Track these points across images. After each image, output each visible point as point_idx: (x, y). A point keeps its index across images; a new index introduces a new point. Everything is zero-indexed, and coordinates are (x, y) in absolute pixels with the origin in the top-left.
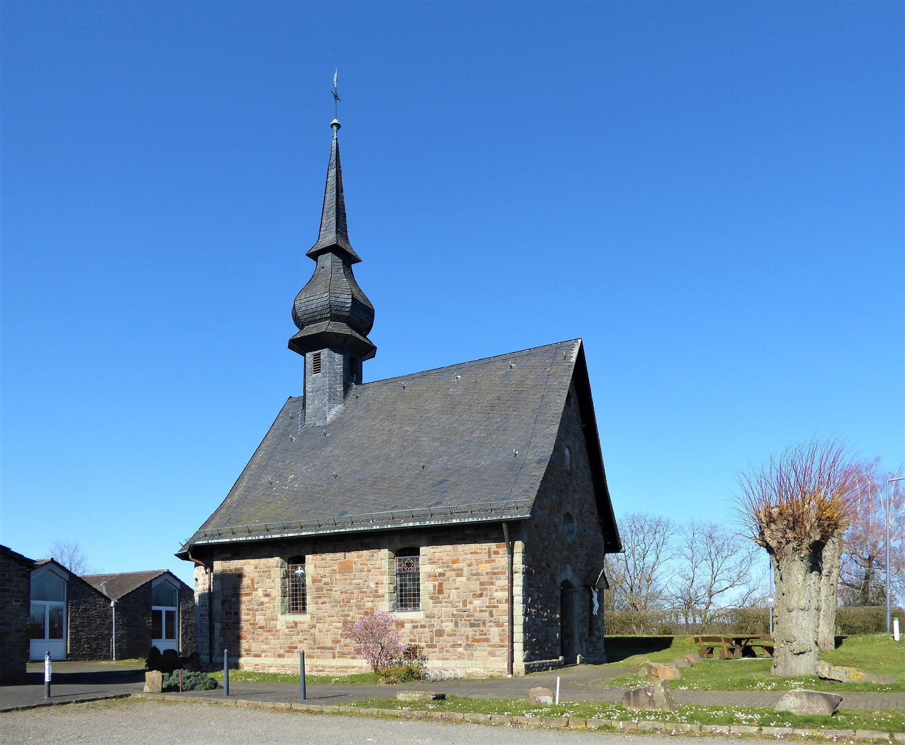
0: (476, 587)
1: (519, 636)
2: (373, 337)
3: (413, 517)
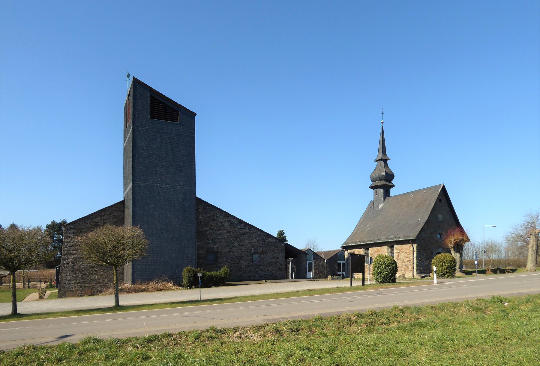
0: (406, 255)
1: (415, 268)
2: (393, 182)
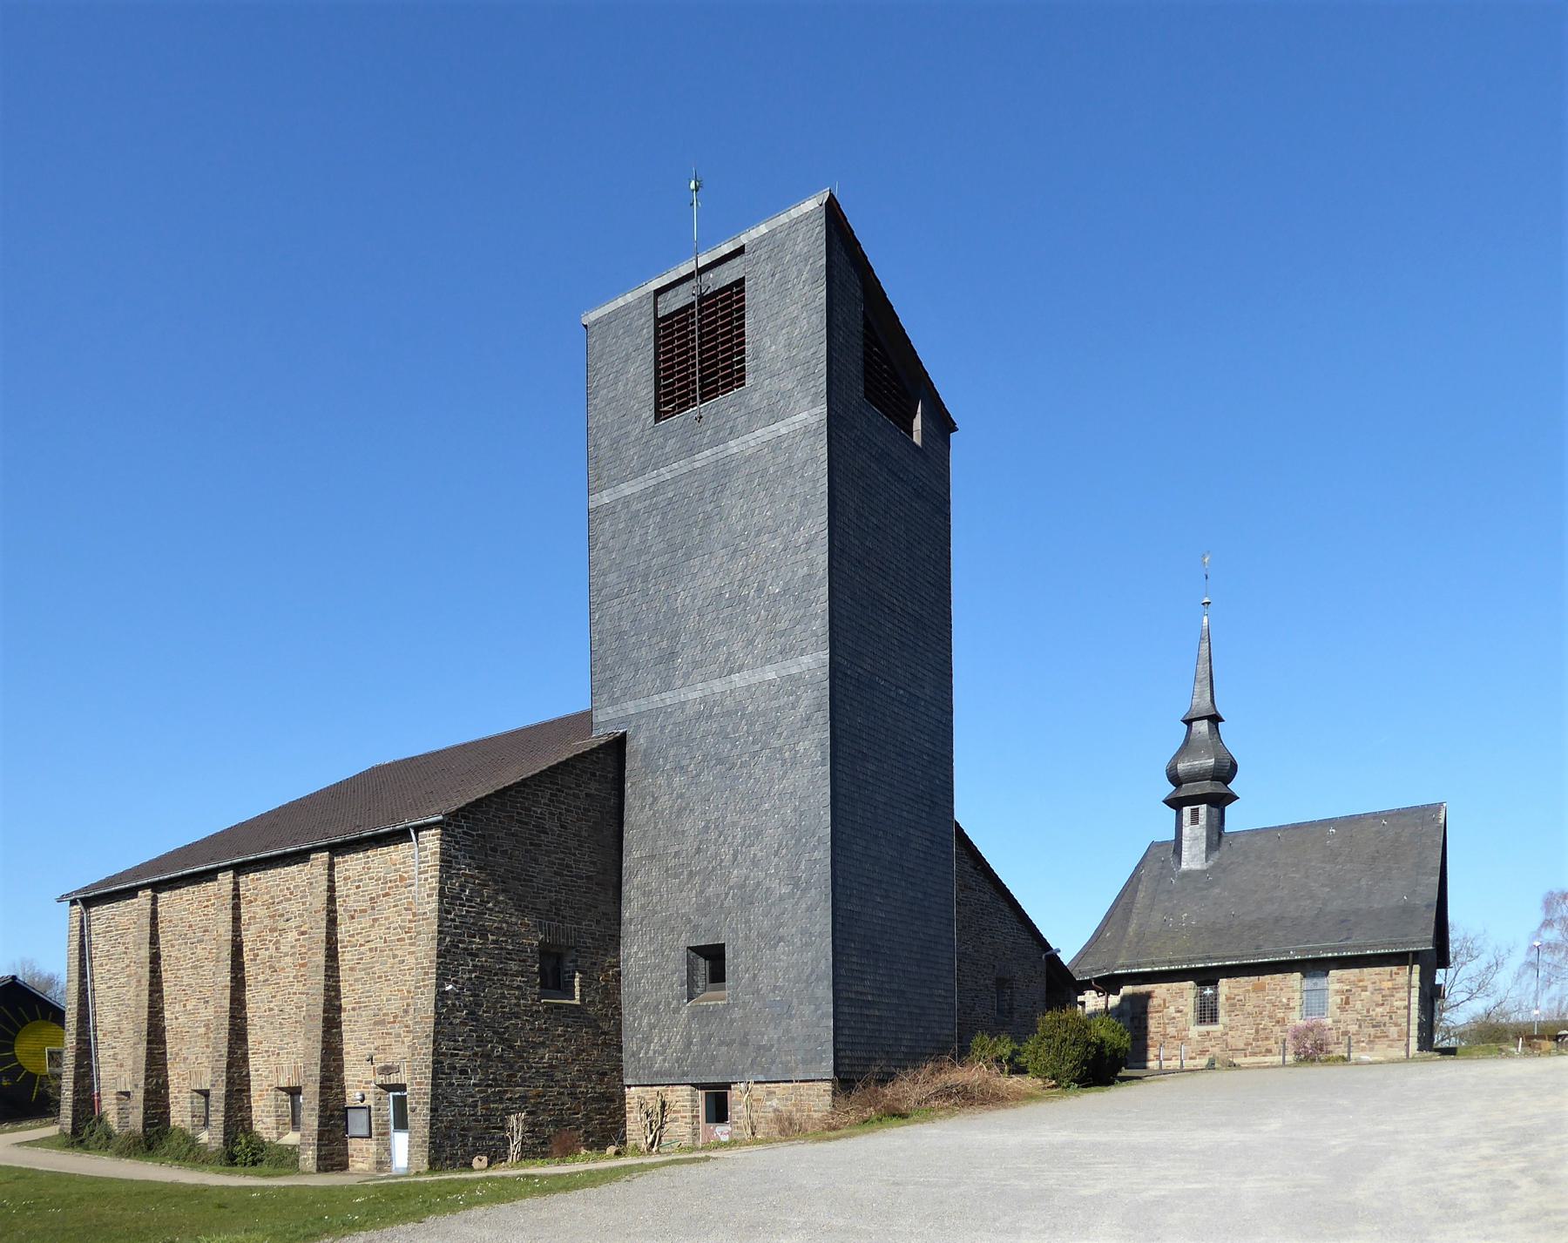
0: (1379, 999)
3: (1333, 949)
